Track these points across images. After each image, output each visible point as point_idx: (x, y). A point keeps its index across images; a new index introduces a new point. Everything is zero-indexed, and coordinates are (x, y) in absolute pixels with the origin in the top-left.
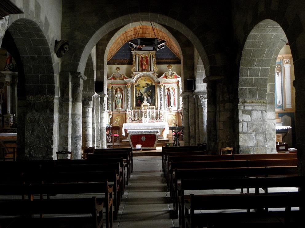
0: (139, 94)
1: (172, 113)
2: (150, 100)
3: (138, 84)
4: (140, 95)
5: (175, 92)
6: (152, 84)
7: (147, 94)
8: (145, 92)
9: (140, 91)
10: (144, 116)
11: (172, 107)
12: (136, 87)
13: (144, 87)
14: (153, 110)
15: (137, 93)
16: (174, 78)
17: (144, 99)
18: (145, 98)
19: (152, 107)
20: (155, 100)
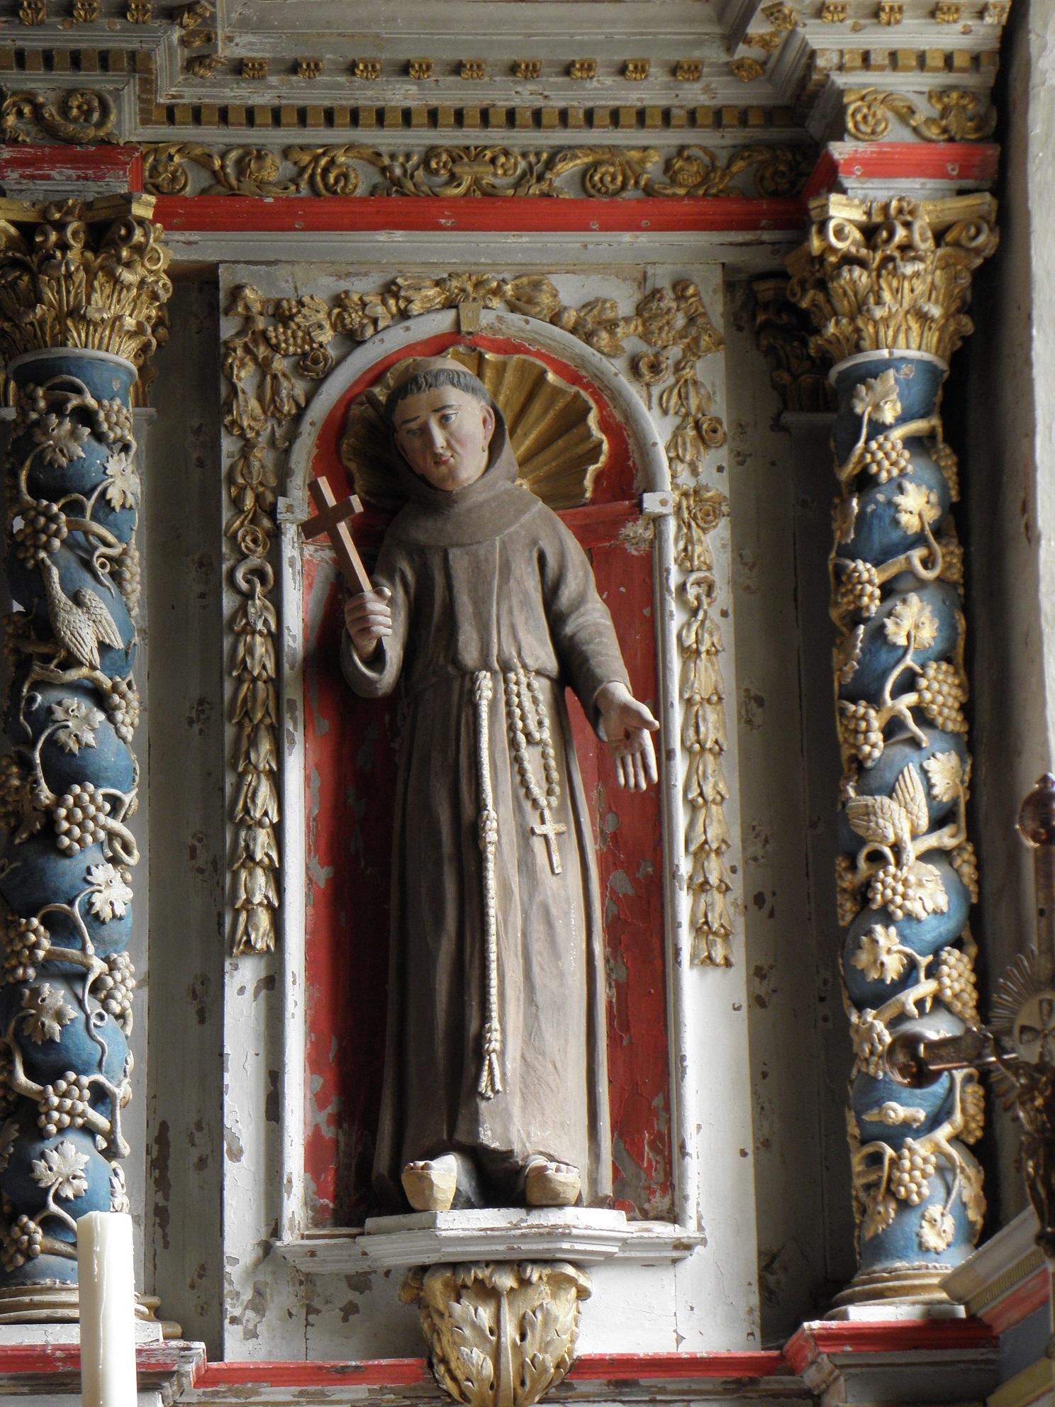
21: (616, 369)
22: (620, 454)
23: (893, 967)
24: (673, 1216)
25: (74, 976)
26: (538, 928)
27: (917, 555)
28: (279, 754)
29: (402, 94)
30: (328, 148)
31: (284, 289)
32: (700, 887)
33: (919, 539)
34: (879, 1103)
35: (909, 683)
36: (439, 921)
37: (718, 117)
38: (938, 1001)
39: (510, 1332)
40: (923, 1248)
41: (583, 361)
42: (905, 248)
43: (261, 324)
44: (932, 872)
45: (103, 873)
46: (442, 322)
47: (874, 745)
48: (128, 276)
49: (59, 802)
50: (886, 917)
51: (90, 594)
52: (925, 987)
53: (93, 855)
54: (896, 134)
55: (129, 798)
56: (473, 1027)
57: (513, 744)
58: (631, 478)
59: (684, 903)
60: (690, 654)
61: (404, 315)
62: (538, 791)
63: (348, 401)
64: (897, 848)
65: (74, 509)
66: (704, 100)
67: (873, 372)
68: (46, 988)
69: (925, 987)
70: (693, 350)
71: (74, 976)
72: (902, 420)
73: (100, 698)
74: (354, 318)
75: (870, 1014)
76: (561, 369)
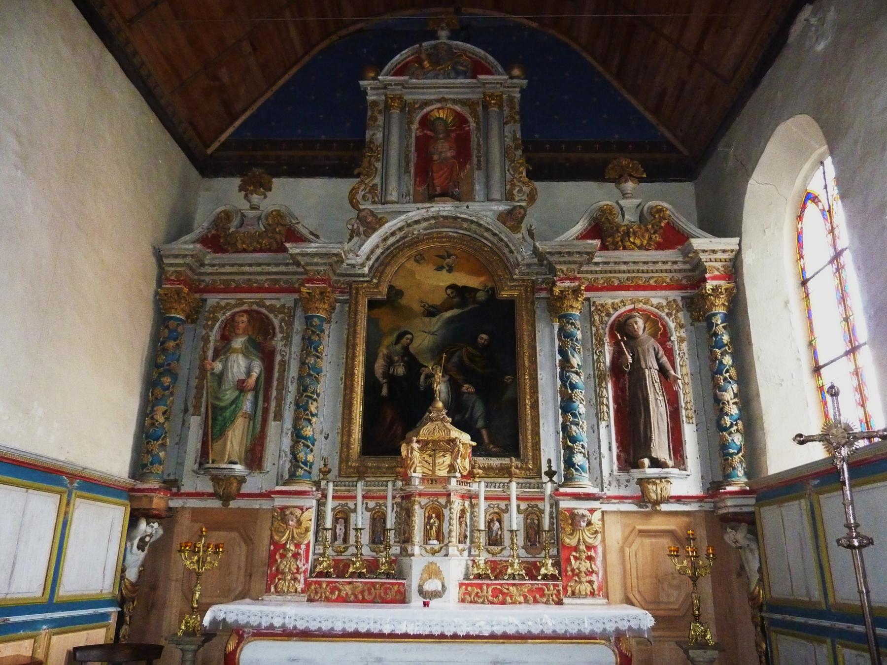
0: (390, 362)
1: (657, 524)
2: (479, 410)
3: (391, 288)
4: (400, 370)
5: (670, 353)
6: (492, 293)
7: (455, 359)
8: (436, 352)
9: (404, 341)
10: (427, 538)
11: (656, 463)
12: (376, 312)
13: (431, 312)
14: (497, 490)
15: (383, 351)
16: (660, 247)
17: (429, 396)
18: (441, 387)
19: (494, 462)
20: (514, 406)
21: (663, 315)
22: (665, 330)
23: (729, 424)
24: (685, 470)
25: (577, 424)
26: (660, 416)
27: (727, 348)
28: (606, 384)
29: (624, 267)
30: (609, 278)
31: (602, 302)
32: (687, 409)
33: (727, 345)
34: (728, 449)
35: (727, 371)
36: (641, 414)
37: (680, 271)
38: (737, 430)
39: (659, 491)
40: (738, 477)
41: (657, 313)
42: (721, 292)
43: (599, 308)
44: (734, 406)
45: (581, 406)
46: (632, 306)
47: (722, 383)
48: (580, 299)
49: (572, 391)
50: (727, 415)
51: (576, 355)
52: (735, 428)
53: (578, 403)
54: (717, 273)
55: (583, 392)
56: (649, 434)
57: (653, 383)
58: (667, 334)
59: (684, 411)
60: (681, 366)
61: (625, 305)
62: (658, 391)
63: (614, 321)
64: (728, 402)
65: (572, 340)
66: (677, 268)
67: (716, 314)
68: (572, 426)
69: (735, 428)
70: (677, 311)
71: (577, 424)
72: (721, 323)
73: (577, 373)
74: (616, 306)
75: (724, 433)
76: (653, 314)
